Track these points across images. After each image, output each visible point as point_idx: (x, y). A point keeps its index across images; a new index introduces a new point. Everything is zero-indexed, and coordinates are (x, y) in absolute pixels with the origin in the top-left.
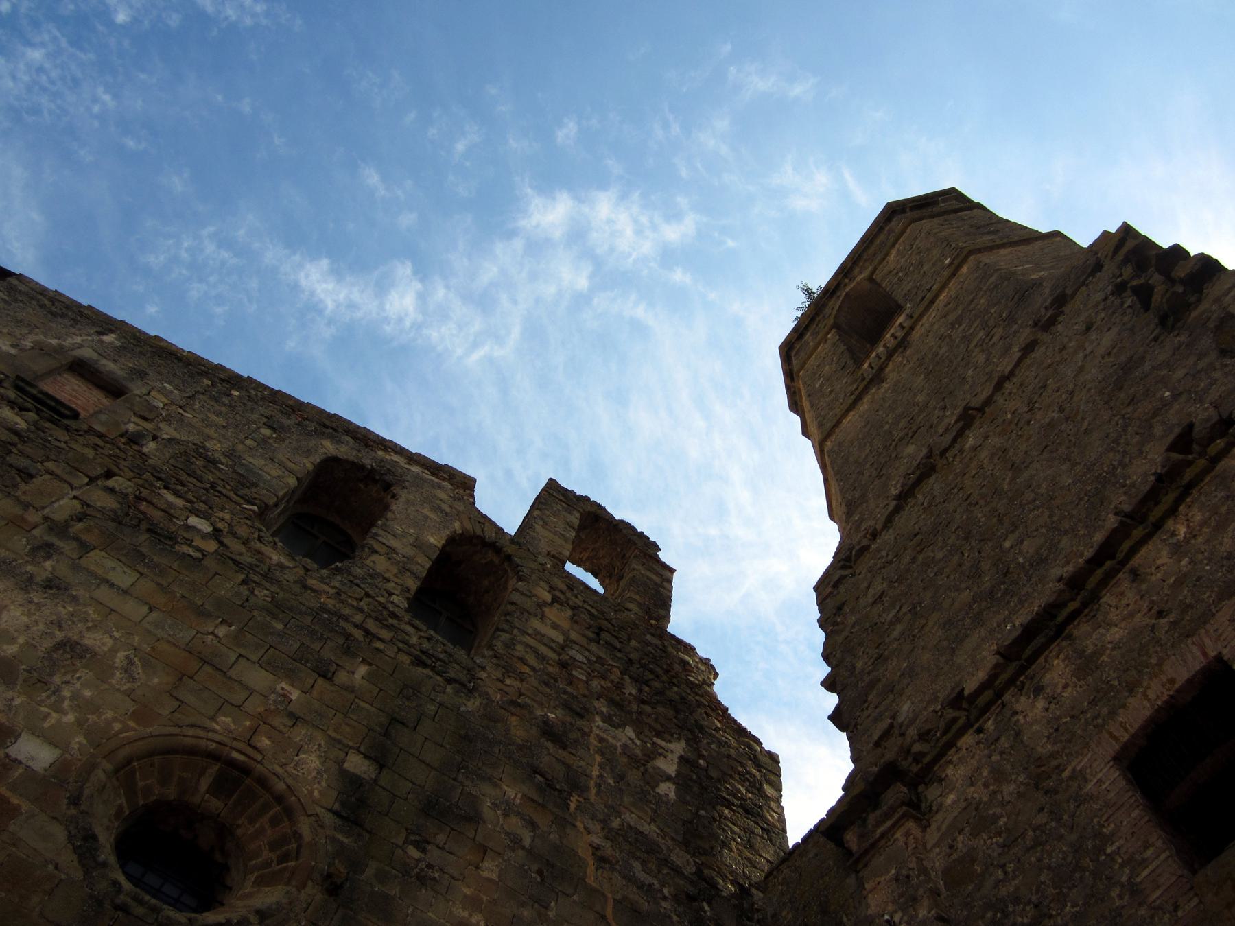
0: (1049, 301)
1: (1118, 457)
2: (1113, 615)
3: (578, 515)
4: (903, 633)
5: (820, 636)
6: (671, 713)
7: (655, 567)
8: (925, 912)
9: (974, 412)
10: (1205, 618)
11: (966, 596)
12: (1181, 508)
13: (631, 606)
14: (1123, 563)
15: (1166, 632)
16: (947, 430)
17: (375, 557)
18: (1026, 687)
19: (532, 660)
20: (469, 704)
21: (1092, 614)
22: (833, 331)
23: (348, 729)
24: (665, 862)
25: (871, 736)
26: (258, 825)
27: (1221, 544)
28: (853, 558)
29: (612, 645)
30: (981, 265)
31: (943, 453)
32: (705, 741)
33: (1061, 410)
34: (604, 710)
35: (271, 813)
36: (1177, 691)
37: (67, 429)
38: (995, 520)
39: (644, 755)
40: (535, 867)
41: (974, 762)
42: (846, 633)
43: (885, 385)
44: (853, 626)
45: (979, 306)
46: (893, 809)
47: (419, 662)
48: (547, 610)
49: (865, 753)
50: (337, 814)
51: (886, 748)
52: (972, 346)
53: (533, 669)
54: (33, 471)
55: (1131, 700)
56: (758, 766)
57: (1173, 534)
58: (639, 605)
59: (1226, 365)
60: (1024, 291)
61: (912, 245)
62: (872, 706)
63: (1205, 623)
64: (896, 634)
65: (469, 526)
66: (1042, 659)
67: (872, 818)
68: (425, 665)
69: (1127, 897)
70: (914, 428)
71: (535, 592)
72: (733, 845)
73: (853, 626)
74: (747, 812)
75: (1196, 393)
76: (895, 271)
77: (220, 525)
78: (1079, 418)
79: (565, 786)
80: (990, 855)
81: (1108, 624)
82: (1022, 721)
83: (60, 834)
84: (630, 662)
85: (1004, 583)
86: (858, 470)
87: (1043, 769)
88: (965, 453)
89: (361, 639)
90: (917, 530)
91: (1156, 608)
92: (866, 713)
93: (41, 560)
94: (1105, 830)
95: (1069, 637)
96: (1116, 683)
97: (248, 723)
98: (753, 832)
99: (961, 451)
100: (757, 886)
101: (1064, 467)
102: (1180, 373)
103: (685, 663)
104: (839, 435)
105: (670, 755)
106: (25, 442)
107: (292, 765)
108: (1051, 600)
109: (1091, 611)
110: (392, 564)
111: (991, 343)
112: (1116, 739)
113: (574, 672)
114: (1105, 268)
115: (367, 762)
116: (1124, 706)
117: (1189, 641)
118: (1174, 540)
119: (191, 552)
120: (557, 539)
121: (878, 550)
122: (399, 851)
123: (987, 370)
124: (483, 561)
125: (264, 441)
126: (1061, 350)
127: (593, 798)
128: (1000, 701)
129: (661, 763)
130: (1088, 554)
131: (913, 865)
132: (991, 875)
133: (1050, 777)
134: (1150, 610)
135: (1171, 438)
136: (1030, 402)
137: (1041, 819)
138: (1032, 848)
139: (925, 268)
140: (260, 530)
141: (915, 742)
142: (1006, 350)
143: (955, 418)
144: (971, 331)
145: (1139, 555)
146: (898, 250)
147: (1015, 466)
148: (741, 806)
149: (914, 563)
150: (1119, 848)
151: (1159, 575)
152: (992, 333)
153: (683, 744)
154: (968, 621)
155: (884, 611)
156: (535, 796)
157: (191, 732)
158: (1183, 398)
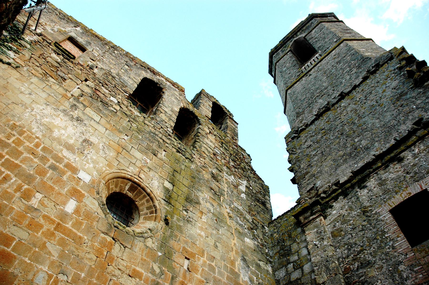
0: (373, 65)
1: (396, 122)
3: (212, 103)
6: (242, 172)
10: (422, 178)
11: (341, 153)
15: (409, 179)
16: (335, 98)
17: (162, 114)
19: (207, 153)
20: (192, 166)
22: (290, 52)
23: (163, 173)
24: (245, 218)
25: (306, 188)
26: (142, 202)
30: (348, 45)
31: (333, 105)
33: (377, 102)
34: (226, 170)
35: (146, 198)
37: (72, 62)
38: (352, 131)
40: (215, 219)
41: (343, 203)
42: (296, 155)
44: (299, 153)
46: (316, 212)
47: (178, 152)
48: (208, 135)
50: (164, 200)
51: (311, 193)
52: (345, 72)
53: (207, 155)
54: (66, 78)
55: (396, 196)
58: (231, 135)
60: (365, 59)
61: (321, 31)
62: (307, 179)
64: (315, 159)
65: (185, 105)
68: (180, 153)
70: (323, 94)
73: (299, 153)
76: (314, 38)
77: (119, 100)
78: (383, 106)
79: (219, 194)
82: (360, 195)
83: (97, 204)
84: (231, 154)
85: (355, 152)
86: (301, 102)
87: (366, 209)
88: (341, 108)
89: (162, 143)
90: (324, 128)
92: (305, 181)
93: (74, 110)
94: (385, 230)
96: (392, 190)
97: (137, 170)
102: (419, 102)
105: (243, 185)
106: (61, 67)
107: (151, 184)
110: (167, 117)
111: (352, 73)
112: (391, 206)
113: (217, 157)
114: (394, 60)
115: (170, 184)
116: (394, 197)
118: (414, 152)
119: (113, 109)
122: (181, 212)
123: (350, 82)
125: (126, 71)
127: (226, 198)
129: (240, 187)
130: (384, 150)
132: (347, 236)
133: (368, 212)
134: (404, 171)
135: (414, 121)
136: (366, 96)
137: (364, 223)
139: (326, 40)
140: (130, 103)
141: (322, 193)
142: (357, 77)
143: (338, 95)
144: (344, 67)
146: (316, 31)
149: (322, 138)
151: (408, 162)
152: (352, 70)
153: (246, 182)
154: (341, 161)
155: (311, 151)
156: (212, 197)
157: (123, 171)
158: (420, 110)
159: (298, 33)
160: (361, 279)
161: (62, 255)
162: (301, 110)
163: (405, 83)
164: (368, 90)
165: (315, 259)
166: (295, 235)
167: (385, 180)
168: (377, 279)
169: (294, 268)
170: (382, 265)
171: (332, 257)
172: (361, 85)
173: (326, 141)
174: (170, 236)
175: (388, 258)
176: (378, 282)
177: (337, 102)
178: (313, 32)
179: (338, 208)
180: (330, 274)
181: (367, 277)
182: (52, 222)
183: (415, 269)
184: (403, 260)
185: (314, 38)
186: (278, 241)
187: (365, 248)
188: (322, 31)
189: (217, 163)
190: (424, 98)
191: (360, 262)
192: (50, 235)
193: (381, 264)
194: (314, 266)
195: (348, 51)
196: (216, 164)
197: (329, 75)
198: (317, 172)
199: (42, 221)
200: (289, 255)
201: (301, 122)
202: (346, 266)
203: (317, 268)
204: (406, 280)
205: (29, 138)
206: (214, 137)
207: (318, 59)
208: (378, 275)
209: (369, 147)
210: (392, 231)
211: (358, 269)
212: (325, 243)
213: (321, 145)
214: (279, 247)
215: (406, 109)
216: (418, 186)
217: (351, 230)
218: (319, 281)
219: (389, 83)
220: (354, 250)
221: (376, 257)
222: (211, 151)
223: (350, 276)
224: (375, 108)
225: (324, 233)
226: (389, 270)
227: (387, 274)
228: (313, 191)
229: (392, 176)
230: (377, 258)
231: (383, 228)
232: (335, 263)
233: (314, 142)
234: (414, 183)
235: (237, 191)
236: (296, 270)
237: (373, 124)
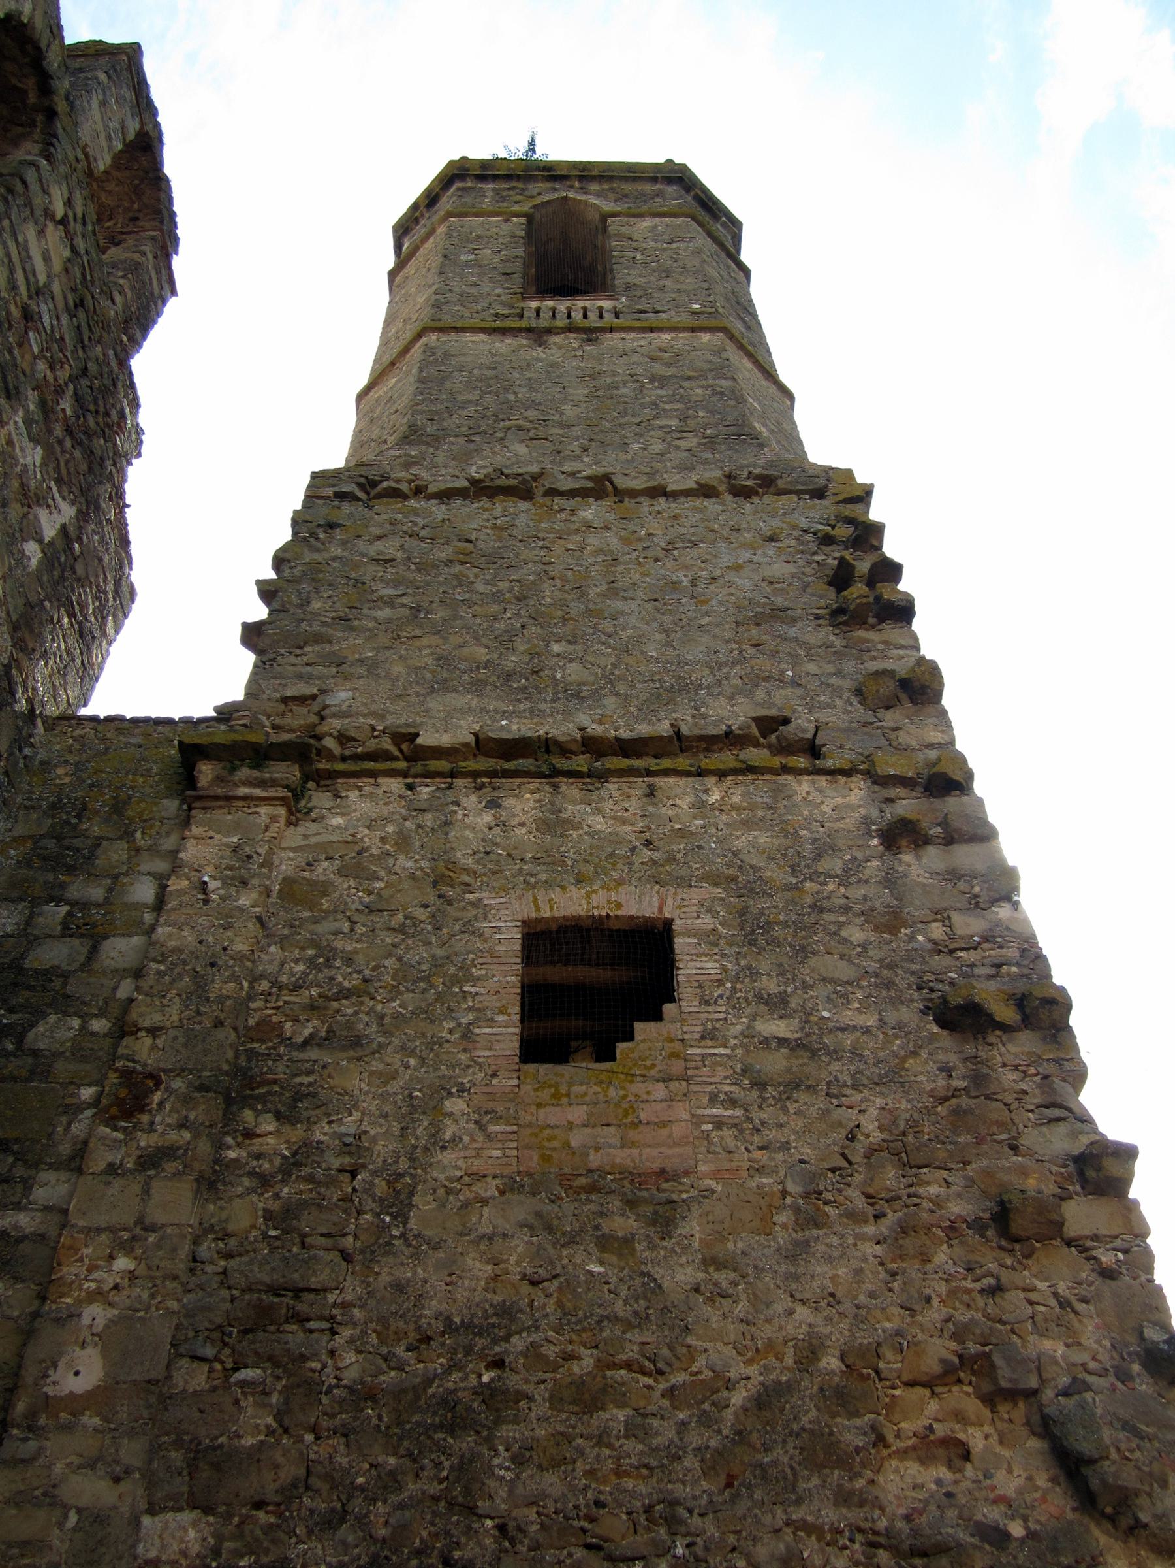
0: (756, 471)
2: (607, 806)
4: (388, 621)
5: (285, 535)
6: (84, 467)
8: (247, 903)
9: (610, 488)
10: (683, 882)
11: (481, 653)
12: (730, 778)
13: (118, 299)
14: (649, 773)
15: (642, 863)
16: (572, 474)
18: (485, 790)
21: (590, 787)
22: (523, 220)
25: (285, 685)
27: (738, 837)
28: (379, 488)
29: (81, 333)
30: (724, 355)
31: (552, 492)
32: (93, 526)
33: (693, 582)
34: (32, 407)
36: (617, 916)
38: (560, 613)
39: (35, 494)
41: (385, 811)
42: (316, 556)
43: (539, 352)
44: (334, 559)
45: (691, 392)
46: (274, 783)
48: (51, 226)
49: (265, 697)
51: (291, 710)
52: (658, 422)
55: (573, 888)
56: (117, 592)
57: (706, 791)
58: (126, 306)
59: (851, 704)
60: (741, 434)
61: (672, 241)
62: (305, 658)
63: (679, 885)
66: (517, 781)
67: (244, 772)
69: (456, 1036)
70: (541, 434)
71: (52, 191)
72: (51, 661)
74: (81, 635)
75: (812, 699)
76: (635, 245)
78: (704, 608)
80: (346, 904)
81: (598, 810)
82: (459, 817)
84: (85, 370)
85: (527, 679)
86: (449, 405)
87: (451, 874)
88: (574, 519)
90: (473, 537)
91: (646, 836)
92: (293, 659)
95: (556, 787)
96: (570, 863)
98: (73, 660)
99: (573, 512)
100: (45, 719)
101: (658, 636)
102: (812, 668)
103: (122, 416)
104: (453, 341)
108: (561, 739)
109: (591, 784)
111: (677, 443)
112: (538, 908)
113: (31, 334)
114: (825, 503)
116: (563, 888)
117: (657, 887)
118: (704, 797)
120: (102, 136)
121: (416, 512)
124: (14, 81)
126: (733, 529)
128: (449, 780)
129: (42, 514)
130: (624, 734)
131: (262, 851)
133: (452, 886)
137: (421, 914)
138: (393, 929)
141: (331, 735)
142: (685, 468)
144: (667, 407)
145: (666, 780)
146: (655, 227)
147: (615, 585)
148: (80, 624)
149: (447, 565)
150: (477, 994)
152: (685, 435)
155: (382, 580)
156: (462, 359)
158: (800, 692)
159: (594, 187)
160: (298, 1080)
162: (431, 429)
163: (809, 590)
164: (692, 530)
165: (170, 935)
166: (141, 815)
167: (568, 821)
168: (353, 1106)
169: (65, 925)
170: (397, 1072)
171: (240, 958)
172: (681, 499)
173: (455, 583)
175: (431, 1056)
176: (351, 1115)
177: (572, 493)
178: (645, 224)
179: (358, 813)
180: (198, 1013)
181: (323, 1083)
183: (492, 1128)
184: (475, 1085)
185: (635, 245)
186: (60, 800)
187: (373, 990)
188: (674, 245)
189: (16, 352)
190: (830, 669)
191: (330, 1026)
193: (397, 1064)
194: (152, 955)
195: (711, 370)
196: (10, 352)
197: (600, 393)
198: (359, 660)
200: (72, 870)
201: (408, 465)
202: (270, 1016)
203: (162, 968)
204: (443, 1148)
206: (67, 253)
207: (601, 317)
208: (366, 1093)
209: (582, 695)
210: (493, 983)
211: (306, 1043)
212: (244, 901)
213: (429, 584)
214: (49, 821)
215: (764, 663)
216: (655, 898)
217: (361, 907)
218: (141, 1015)
219: (765, 555)
220: (332, 979)
221: (391, 1034)
222: (23, 289)
223: (264, 1054)
224: (675, 597)
225: (262, 865)
226: (410, 1096)
227: (396, 1102)
228: (303, 710)
229: (599, 823)
230: (396, 1042)
231: (473, 960)
232: (241, 983)
233: (409, 558)
234: (650, 882)
235: (25, 515)
236: (70, 936)
237: (640, 637)
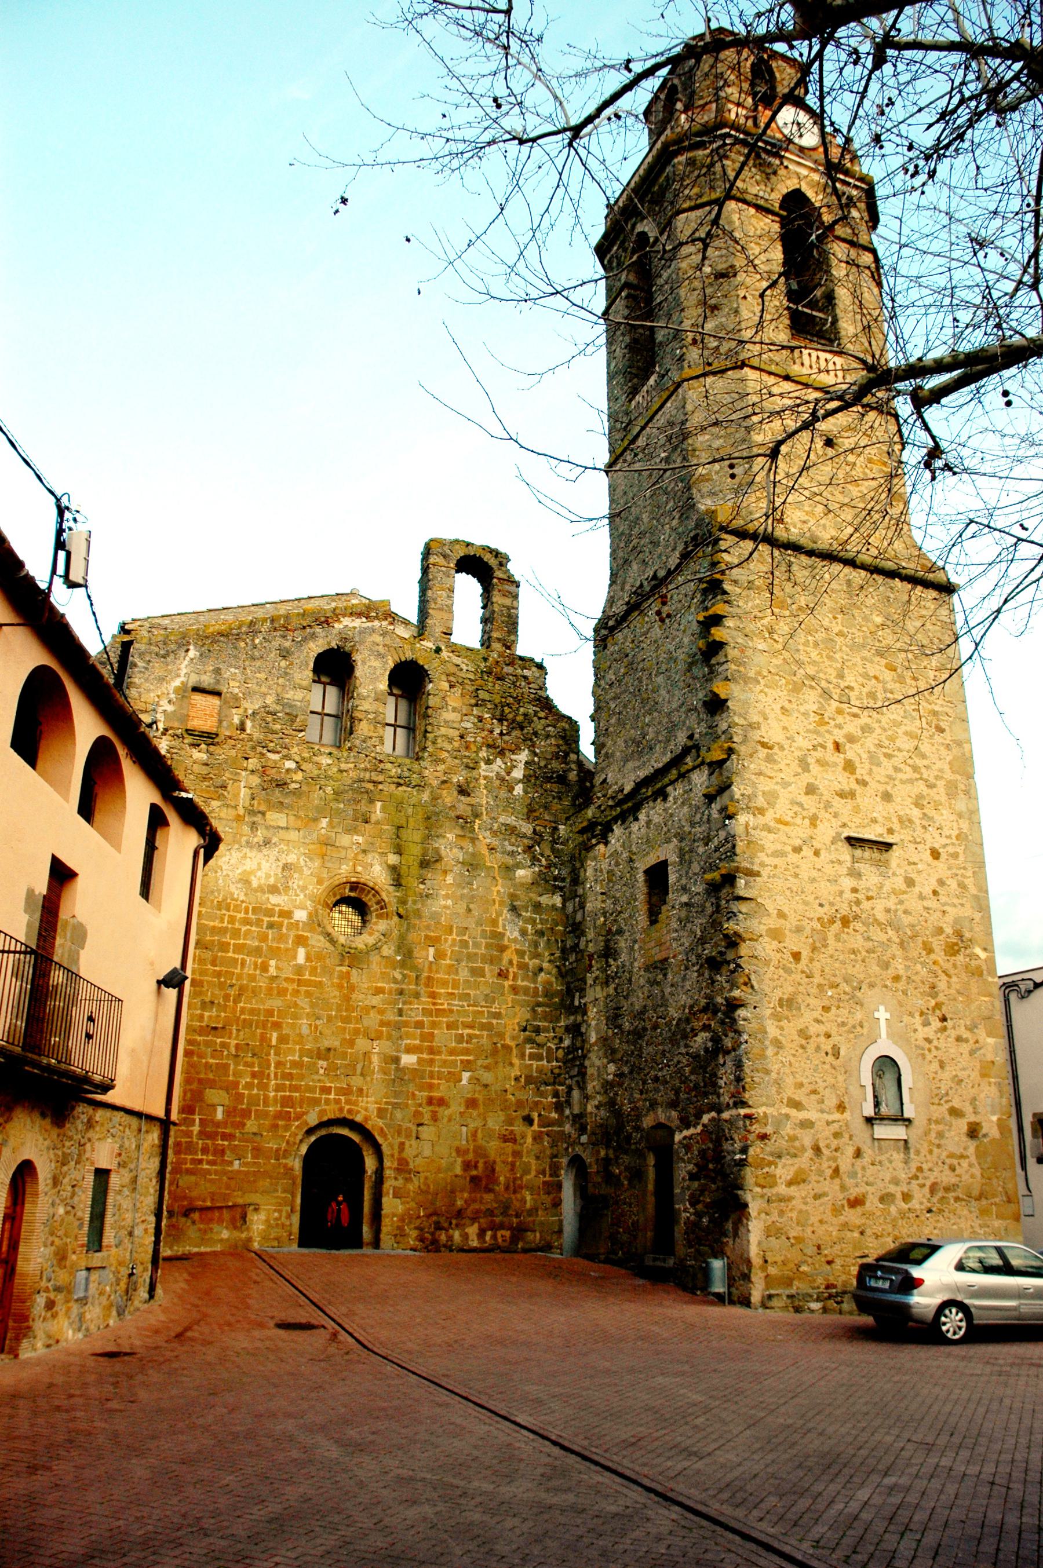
7: (530, 1419)
83: (322, 938)
161: (312, 1005)
174: (408, 930)
182: (292, 980)
192: (297, 992)
199: (285, 985)
205: (237, 909)
